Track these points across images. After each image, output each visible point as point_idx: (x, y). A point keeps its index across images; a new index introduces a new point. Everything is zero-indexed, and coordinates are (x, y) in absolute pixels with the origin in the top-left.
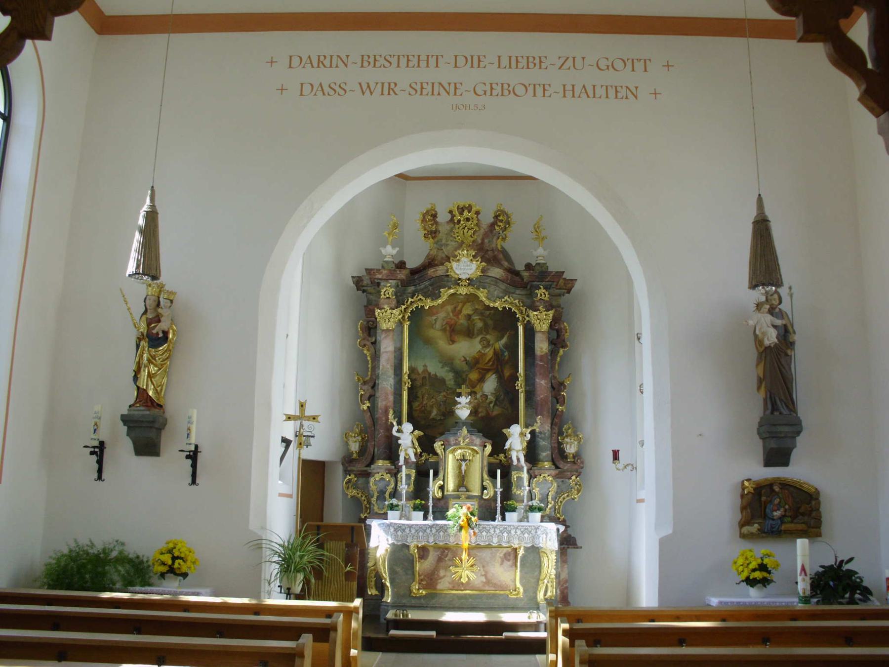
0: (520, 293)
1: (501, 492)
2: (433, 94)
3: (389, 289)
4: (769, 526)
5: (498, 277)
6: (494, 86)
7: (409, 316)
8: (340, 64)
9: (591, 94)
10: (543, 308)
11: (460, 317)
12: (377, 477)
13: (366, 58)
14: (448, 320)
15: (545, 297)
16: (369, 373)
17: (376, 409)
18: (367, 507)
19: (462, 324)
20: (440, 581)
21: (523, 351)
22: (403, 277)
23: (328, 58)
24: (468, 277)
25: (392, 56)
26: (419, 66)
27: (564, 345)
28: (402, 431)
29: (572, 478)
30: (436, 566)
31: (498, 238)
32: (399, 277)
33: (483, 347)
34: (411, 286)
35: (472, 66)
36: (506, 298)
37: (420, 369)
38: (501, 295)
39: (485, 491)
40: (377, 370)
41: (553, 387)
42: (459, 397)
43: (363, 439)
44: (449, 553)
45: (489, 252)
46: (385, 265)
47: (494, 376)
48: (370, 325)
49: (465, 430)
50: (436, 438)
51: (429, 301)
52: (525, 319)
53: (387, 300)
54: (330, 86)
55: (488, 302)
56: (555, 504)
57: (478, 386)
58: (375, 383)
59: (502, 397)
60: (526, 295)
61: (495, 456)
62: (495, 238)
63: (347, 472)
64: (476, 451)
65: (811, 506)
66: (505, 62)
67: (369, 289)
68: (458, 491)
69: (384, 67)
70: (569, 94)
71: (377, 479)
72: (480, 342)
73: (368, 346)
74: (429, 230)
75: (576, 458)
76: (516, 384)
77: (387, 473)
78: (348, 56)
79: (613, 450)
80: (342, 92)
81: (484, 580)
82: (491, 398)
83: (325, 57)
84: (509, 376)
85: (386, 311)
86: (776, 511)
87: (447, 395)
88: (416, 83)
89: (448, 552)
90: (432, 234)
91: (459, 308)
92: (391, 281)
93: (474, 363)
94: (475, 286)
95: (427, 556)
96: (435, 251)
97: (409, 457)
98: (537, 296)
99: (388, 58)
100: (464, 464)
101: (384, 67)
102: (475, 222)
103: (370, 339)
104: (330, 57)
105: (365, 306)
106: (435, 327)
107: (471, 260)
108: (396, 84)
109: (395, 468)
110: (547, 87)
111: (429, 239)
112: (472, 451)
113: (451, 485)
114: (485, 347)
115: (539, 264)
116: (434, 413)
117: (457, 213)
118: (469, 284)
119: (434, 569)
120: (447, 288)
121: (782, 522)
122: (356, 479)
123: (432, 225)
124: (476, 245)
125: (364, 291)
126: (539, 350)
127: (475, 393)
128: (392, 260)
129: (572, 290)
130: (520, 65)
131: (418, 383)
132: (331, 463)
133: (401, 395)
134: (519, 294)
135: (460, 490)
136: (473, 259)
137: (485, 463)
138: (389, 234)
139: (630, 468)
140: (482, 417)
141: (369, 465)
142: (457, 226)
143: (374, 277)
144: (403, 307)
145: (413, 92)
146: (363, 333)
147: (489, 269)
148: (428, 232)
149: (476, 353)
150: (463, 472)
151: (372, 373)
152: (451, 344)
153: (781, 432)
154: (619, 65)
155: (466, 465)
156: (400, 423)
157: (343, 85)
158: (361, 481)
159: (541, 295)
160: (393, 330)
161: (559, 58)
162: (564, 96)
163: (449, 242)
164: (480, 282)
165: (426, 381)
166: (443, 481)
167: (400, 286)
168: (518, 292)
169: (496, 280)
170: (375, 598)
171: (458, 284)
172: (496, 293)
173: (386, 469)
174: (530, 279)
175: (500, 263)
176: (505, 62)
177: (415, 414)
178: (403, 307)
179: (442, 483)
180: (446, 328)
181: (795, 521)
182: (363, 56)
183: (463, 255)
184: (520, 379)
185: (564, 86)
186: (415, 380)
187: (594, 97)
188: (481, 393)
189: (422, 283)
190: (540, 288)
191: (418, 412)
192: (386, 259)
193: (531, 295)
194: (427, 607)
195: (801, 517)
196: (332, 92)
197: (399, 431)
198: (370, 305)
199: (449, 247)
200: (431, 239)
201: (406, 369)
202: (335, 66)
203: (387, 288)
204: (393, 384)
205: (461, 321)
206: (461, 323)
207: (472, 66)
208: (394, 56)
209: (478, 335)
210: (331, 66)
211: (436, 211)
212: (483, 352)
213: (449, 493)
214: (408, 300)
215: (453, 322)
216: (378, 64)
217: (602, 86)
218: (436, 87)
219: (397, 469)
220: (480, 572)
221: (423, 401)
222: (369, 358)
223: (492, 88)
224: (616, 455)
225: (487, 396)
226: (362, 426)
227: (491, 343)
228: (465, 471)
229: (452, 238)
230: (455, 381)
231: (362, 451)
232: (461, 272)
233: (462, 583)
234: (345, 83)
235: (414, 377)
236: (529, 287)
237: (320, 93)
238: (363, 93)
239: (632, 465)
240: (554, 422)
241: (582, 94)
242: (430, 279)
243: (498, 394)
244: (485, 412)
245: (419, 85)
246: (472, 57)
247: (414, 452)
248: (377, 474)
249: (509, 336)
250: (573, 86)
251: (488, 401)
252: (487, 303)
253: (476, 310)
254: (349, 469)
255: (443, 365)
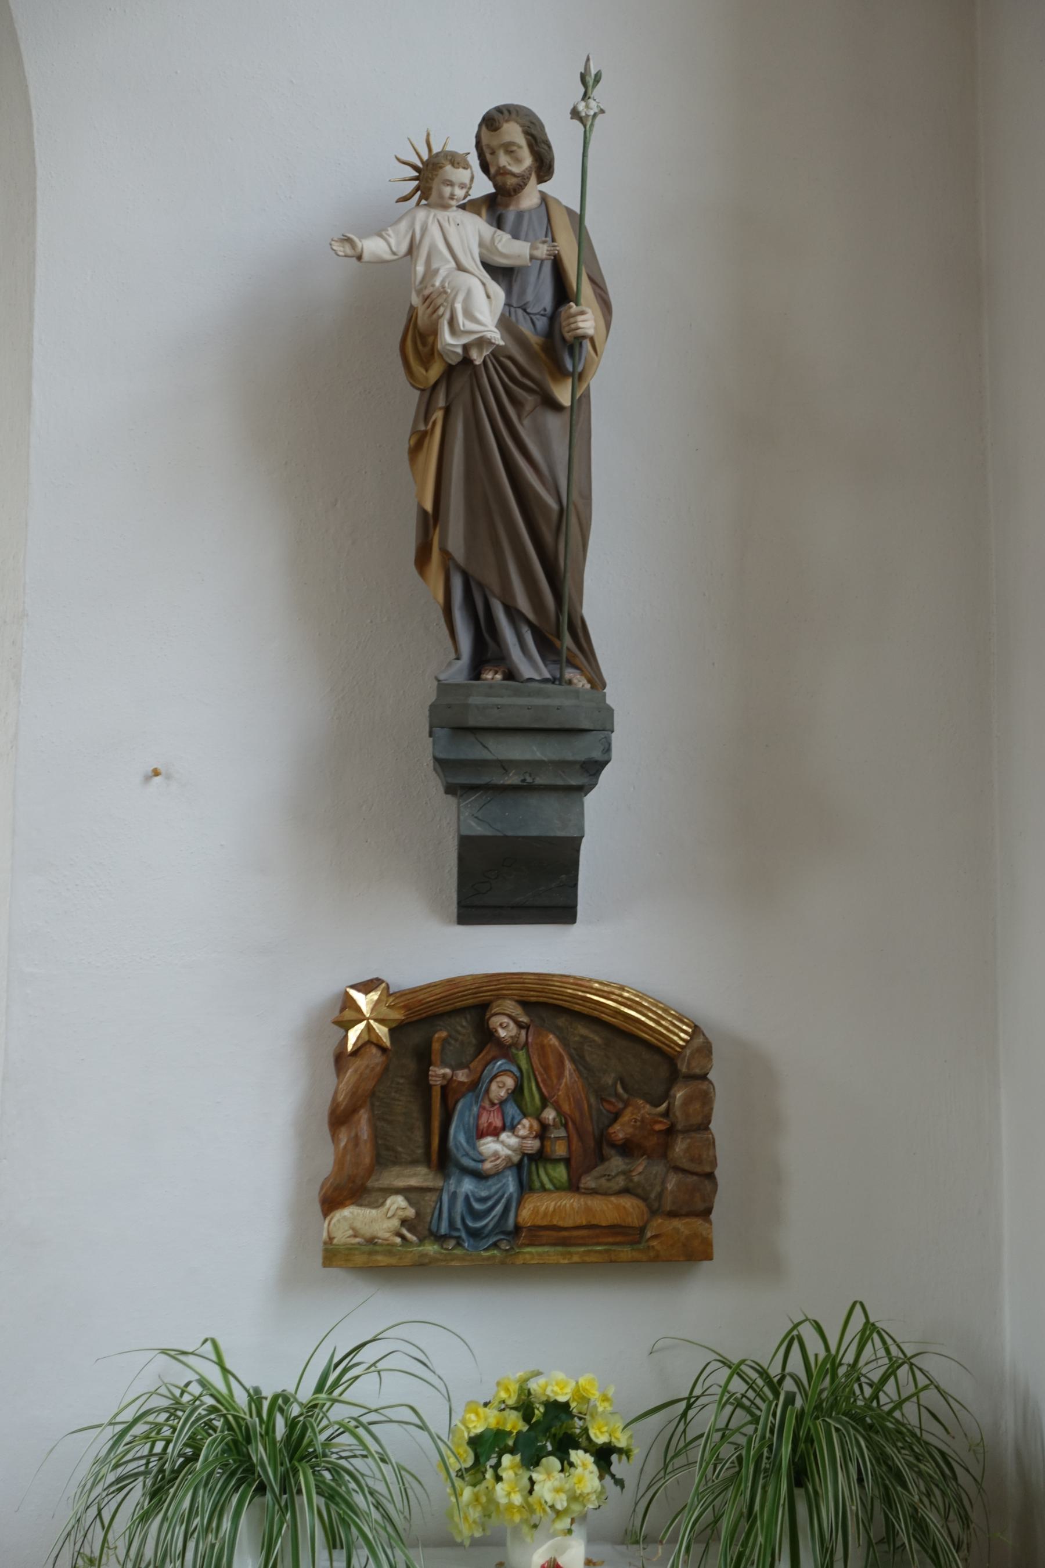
4: (460, 1206)
65: (666, 1114)
86: (496, 1133)
121: (525, 1187)
153: (504, 766)
181: (588, 1181)
195: (617, 1163)
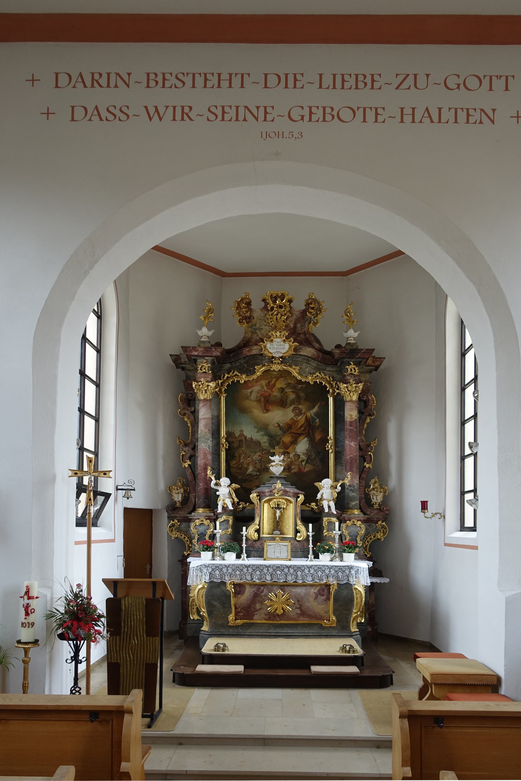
0: (332, 370)
1: (313, 536)
2: (237, 120)
3: (205, 365)
5: (310, 356)
6: (314, 110)
7: (225, 389)
8: (120, 83)
9: (435, 118)
10: (353, 381)
11: (274, 390)
12: (198, 522)
13: (152, 76)
14: (263, 393)
15: (355, 372)
16: (190, 437)
17: (196, 467)
18: (189, 546)
19: (275, 396)
20: (256, 613)
21: (333, 416)
22: (219, 354)
23: (105, 76)
24: (281, 355)
25: (186, 74)
26: (219, 86)
27: (371, 414)
28: (220, 484)
29: (378, 522)
30: (253, 601)
31: (310, 323)
32: (214, 354)
33: (295, 416)
34: (227, 363)
35: (286, 87)
36: (318, 374)
37: (237, 434)
38: (312, 371)
39: (298, 534)
40: (196, 434)
41: (360, 449)
42: (273, 457)
43: (185, 491)
44: (265, 590)
45: (301, 335)
46: (202, 345)
47: (306, 439)
48: (189, 398)
49: (279, 485)
50: (253, 490)
51: (244, 376)
52: (335, 392)
53: (203, 375)
54: (108, 110)
55: (300, 377)
56: (363, 543)
57: (291, 448)
58: (195, 445)
59: (314, 456)
60: (336, 371)
61: (308, 505)
62: (307, 323)
63: (170, 518)
64: (290, 501)
66: (327, 81)
67: (187, 366)
68: (272, 534)
69: (176, 87)
70: (408, 119)
71: (197, 524)
72: (293, 411)
73: (187, 414)
74: (244, 315)
75: (382, 507)
76: (326, 446)
77: (206, 519)
78: (129, 74)
79: (421, 502)
80: (123, 117)
81: (299, 612)
82: (303, 457)
83: (101, 75)
84: (320, 439)
85: (203, 384)
87: (263, 455)
88: (216, 107)
89: (264, 589)
90: (247, 319)
91: (273, 382)
92: (207, 358)
93: (287, 428)
94: (288, 364)
95: (244, 592)
96: (250, 334)
97: (227, 505)
98: (348, 371)
99: (180, 76)
100: (278, 512)
101: (176, 87)
102: (288, 309)
103: (189, 408)
104: (106, 75)
105: (184, 381)
106: (251, 399)
107: (284, 340)
108: (191, 108)
109: (214, 515)
110: (380, 111)
111: (244, 323)
112: (286, 501)
113: (266, 527)
114: (297, 415)
115: (349, 343)
116: (251, 469)
117: (271, 302)
118: (282, 362)
119: (251, 603)
120: (261, 366)
122: (179, 523)
123: (247, 312)
124: (288, 329)
125: (183, 369)
126: (348, 416)
127: (288, 453)
128: (209, 340)
129: (380, 368)
130: (347, 85)
131: (236, 445)
132: (157, 510)
133: (219, 455)
134: (330, 371)
135: (274, 533)
136: (286, 340)
137: (299, 510)
138: (205, 318)
139: (439, 516)
140: (295, 473)
141: (190, 513)
142: (270, 313)
143: (190, 354)
144: (220, 382)
145: (212, 117)
146: (183, 404)
147: (301, 349)
148: (243, 317)
149: (289, 420)
150: (278, 518)
151: (192, 437)
152: (265, 413)
154: (472, 83)
155: (281, 512)
156: (218, 477)
157: (125, 109)
158: (184, 525)
159: (351, 370)
160: (210, 400)
161: (397, 75)
162: (402, 121)
163: (263, 327)
164: (292, 360)
165: (243, 443)
166: (259, 525)
167: (216, 364)
168: (328, 369)
169: (308, 359)
170: (197, 622)
171: (272, 362)
172: (307, 369)
173: (206, 516)
174: (341, 356)
175: (311, 344)
176: (327, 81)
177: (233, 470)
178: (220, 382)
179: (258, 527)
180: (260, 399)
182: (148, 74)
183: (276, 336)
184: (330, 442)
185: (402, 109)
186: (233, 442)
187: (440, 121)
188: (294, 453)
189: (237, 361)
190: (351, 364)
191: (236, 468)
192: (202, 340)
193: (341, 371)
194: (244, 635)
196: (111, 117)
197: (217, 484)
198: (189, 380)
199: (263, 331)
200: (246, 324)
201: (223, 433)
202: (114, 85)
203: (204, 365)
204: (211, 446)
205: (275, 394)
206: (275, 395)
207: (286, 87)
208: (188, 74)
209: (291, 405)
210: (108, 86)
211: (250, 300)
212: (295, 419)
213: (264, 536)
214: (224, 376)
215: (267, 394)
216: (167, 84)
217: (450, 109)
218: (241, 110)
219: (216, 516)
220: (295, 605)
221: (240, 459)
222: (189, 425)
223: (311, 113)
224: (424, 505)
225: (299, 456)
226: (184, 480)
227: (303, 411)
228: (280, 517)
229: (265, 323)
230: (270, 444)
231: (185, 500)
232: (275, 350)
233: (278, 615)
234: (128, 107)
235: (231, 440)
236: (339, 364)
237: (96, 118)
238: (151, 119)
239: (440, 514)
240: (362, 477)
241: (423, 118)
242: (245, 358)
243: (310, 454)
244: (297, 468)
245: (220, 109)
246: (286, 75)
247: (231, 502)
248: (198, 520)
249: (319, 406)
250: (413, 109)
251: (300, 460)
252: (299, 378)
253: (288, 385)
254: (172, 515)
255: (258, 430)
